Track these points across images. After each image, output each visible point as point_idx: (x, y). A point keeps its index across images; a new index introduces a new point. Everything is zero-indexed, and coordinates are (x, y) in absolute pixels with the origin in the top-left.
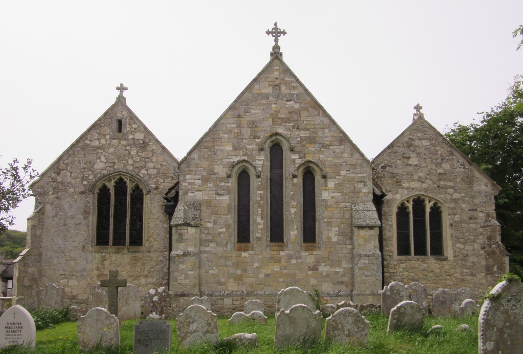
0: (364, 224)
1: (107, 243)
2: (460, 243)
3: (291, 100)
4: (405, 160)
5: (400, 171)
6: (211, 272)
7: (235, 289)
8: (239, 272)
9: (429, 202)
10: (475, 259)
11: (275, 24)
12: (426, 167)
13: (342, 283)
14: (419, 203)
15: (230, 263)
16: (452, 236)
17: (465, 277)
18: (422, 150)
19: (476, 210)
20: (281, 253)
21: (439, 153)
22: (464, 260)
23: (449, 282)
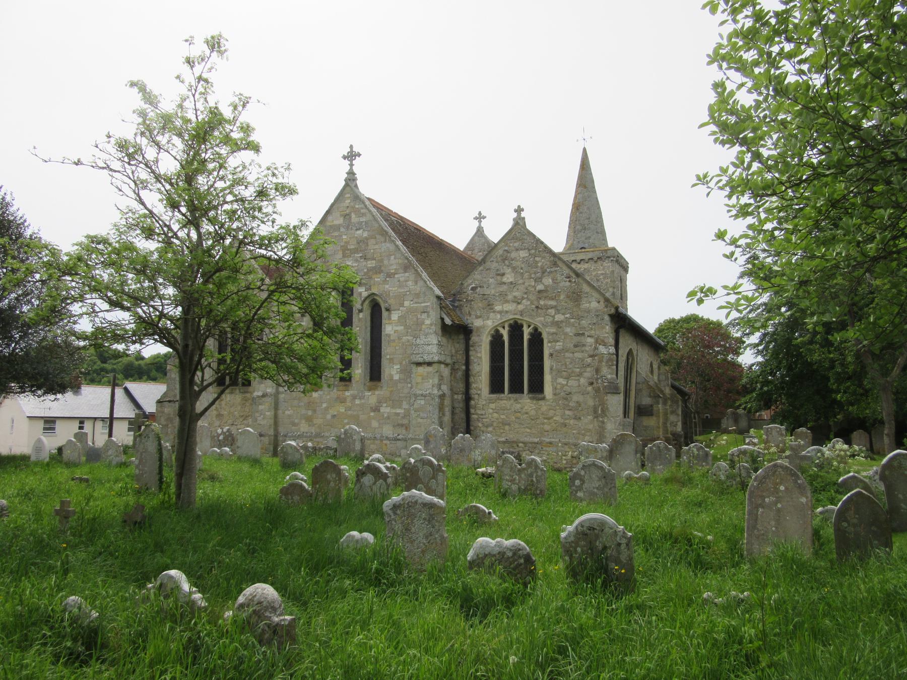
0: (421, 360)
1: (503, 392)
2: (562, 377)
3: (359, 229)
4: (499, 278)
5: (493, 292)
6: (287, 412)
7: (306, 430)
8: (310, 413)
9: (504, 328)
10: (580, 398)
11: (351, 147)
12: (524, 283)
13: (402, 425)
14: (516, 329)
15: (302, 404)
16: (551, 369)
17: (567, 421)
18: (518, 263)
19: (583, 334)
20: (347, 394)
21: (539, 265)
22: (566, 399)
23: (547, 427)
